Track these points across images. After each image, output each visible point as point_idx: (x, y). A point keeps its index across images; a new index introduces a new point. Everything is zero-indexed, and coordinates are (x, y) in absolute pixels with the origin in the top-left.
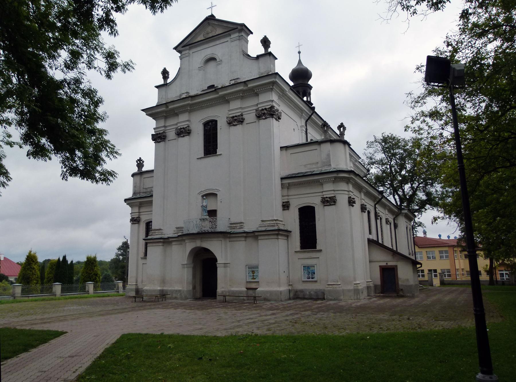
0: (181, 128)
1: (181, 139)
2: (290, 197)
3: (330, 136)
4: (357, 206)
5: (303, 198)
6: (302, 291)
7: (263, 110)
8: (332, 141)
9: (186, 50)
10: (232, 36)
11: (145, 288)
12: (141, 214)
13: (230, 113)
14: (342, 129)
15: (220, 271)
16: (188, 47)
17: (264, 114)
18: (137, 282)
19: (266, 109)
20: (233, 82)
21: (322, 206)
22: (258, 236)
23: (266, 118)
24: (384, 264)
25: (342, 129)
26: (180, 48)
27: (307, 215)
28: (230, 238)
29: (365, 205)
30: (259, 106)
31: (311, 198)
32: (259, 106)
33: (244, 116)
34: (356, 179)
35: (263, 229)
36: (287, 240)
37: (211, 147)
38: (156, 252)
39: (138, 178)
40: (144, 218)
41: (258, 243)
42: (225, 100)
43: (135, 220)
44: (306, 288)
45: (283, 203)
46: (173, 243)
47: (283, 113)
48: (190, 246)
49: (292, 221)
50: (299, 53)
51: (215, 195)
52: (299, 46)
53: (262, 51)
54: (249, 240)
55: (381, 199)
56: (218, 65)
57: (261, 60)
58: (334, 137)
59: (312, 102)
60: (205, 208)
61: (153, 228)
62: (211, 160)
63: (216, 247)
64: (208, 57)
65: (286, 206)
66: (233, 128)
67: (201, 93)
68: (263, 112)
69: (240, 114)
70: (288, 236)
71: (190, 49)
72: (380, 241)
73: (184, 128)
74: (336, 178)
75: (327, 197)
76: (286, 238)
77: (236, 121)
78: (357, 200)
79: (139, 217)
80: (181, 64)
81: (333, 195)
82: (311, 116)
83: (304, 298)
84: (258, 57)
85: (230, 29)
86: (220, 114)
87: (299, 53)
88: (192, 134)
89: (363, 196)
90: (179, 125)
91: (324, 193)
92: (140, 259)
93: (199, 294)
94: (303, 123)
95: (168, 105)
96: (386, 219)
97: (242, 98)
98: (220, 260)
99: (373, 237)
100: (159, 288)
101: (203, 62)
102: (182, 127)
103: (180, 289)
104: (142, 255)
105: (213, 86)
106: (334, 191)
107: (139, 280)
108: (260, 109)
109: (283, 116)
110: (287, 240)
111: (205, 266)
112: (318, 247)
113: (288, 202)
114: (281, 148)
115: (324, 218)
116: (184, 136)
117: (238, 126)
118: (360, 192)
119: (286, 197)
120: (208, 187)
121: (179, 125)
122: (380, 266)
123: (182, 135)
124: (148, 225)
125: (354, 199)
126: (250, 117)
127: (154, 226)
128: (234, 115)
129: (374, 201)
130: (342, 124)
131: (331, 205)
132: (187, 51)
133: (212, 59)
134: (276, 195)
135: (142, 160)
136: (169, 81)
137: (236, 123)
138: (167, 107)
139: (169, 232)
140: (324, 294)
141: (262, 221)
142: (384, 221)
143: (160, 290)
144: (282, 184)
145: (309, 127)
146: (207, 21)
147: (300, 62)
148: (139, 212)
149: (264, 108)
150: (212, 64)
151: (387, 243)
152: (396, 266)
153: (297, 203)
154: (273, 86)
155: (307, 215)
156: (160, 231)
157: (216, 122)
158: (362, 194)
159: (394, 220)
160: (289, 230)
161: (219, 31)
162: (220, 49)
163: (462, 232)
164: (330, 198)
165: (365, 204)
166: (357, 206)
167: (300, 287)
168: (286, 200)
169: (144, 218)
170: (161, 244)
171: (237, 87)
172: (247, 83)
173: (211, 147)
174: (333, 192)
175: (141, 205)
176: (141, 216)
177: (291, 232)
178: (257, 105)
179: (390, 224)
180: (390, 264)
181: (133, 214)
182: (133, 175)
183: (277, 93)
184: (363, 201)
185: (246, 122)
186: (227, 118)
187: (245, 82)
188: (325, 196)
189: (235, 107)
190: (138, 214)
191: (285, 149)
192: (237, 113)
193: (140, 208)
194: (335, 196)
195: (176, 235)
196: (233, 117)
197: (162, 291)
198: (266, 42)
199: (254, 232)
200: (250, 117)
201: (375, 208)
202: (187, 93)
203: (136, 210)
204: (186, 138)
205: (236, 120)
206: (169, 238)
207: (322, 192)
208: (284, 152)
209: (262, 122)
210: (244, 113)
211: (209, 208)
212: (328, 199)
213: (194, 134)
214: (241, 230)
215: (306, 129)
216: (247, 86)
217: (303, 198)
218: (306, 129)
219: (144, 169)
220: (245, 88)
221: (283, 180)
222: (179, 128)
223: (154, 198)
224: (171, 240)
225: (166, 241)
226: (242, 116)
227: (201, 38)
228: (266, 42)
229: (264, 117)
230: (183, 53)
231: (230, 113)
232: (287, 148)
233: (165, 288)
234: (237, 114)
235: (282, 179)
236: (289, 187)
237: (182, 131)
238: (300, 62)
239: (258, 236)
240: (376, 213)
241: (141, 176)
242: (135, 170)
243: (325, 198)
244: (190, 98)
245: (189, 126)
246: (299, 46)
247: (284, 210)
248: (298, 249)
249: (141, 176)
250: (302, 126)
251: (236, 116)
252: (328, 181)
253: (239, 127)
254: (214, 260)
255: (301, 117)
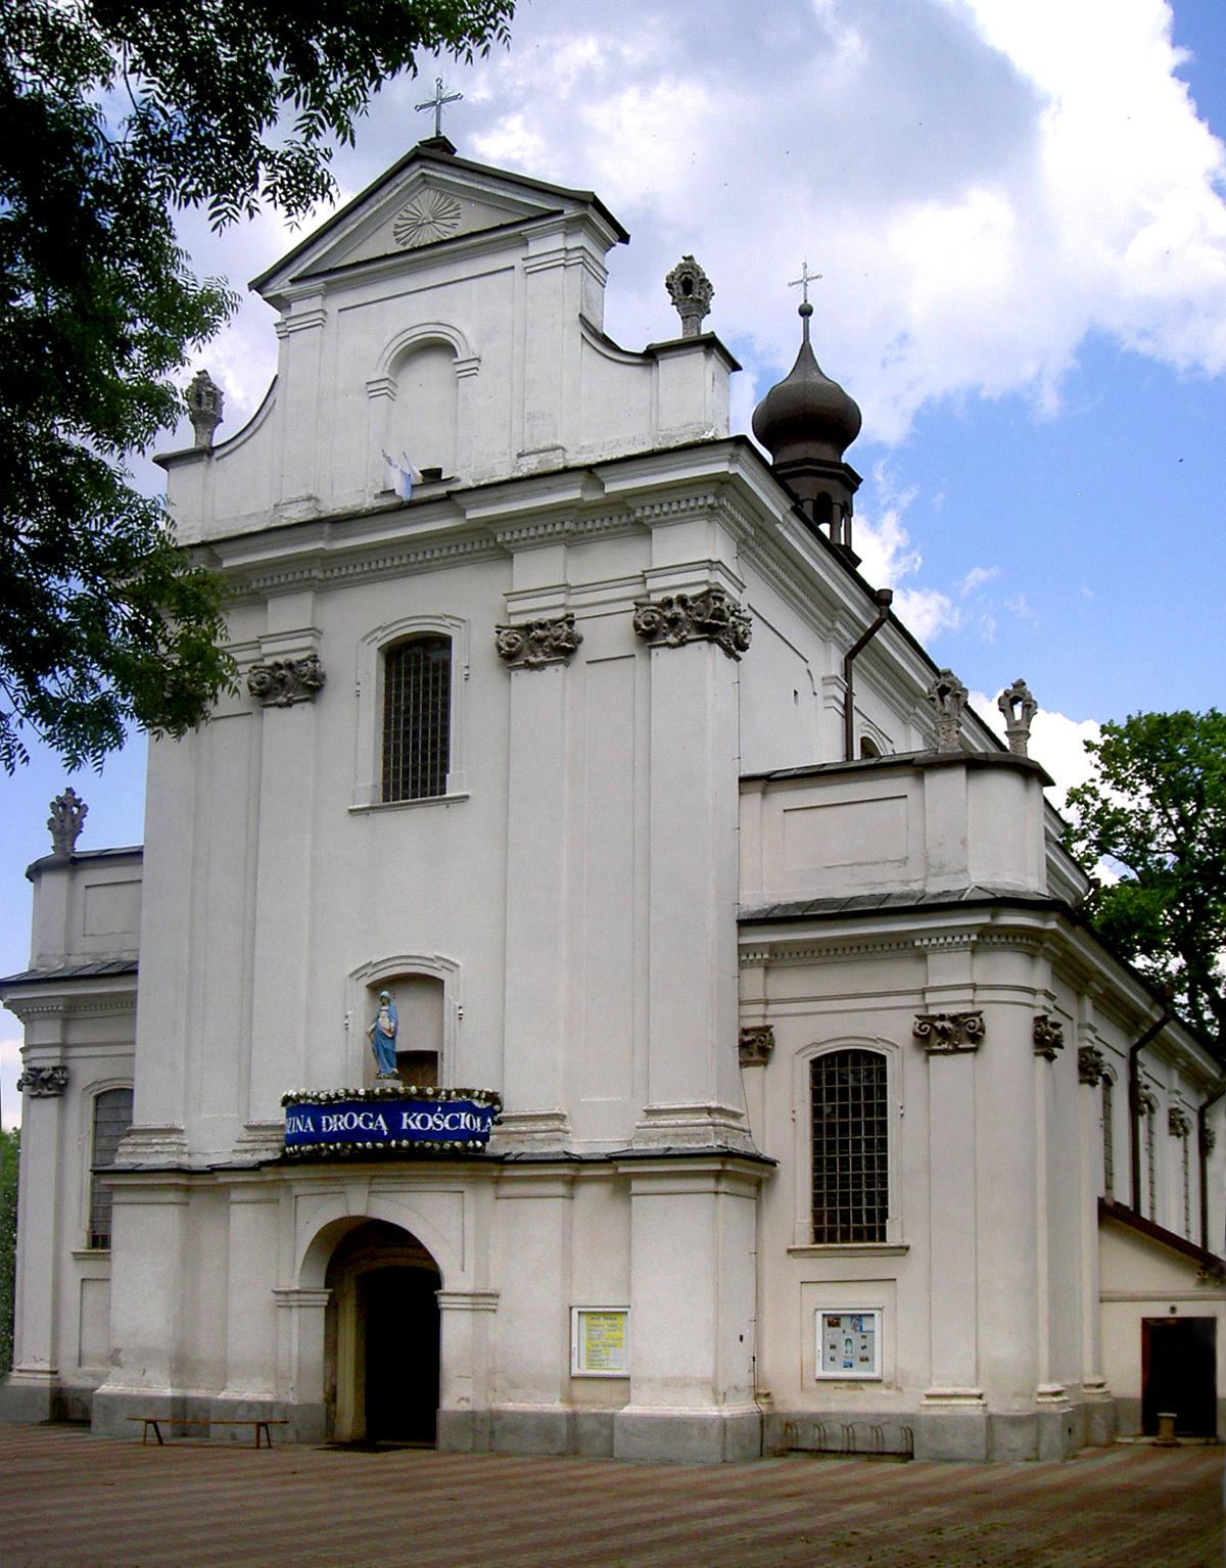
0: (278, 666)
1: (272, 714)
2: (773, 1009)
3: (963, 742)
4: (1067, 1057)
5: (822, 1014)
6: (816, 1421)
7: (668, 603)
8: (975, 765)
9: (309, 296)
10: (535, 248)
11: (105, 1389)
12: (74, 1052)
13: (513, 607)
14: (1018, 709)
15: (455, 1331)
16: (319, 283)
17: (674, 622)
18: (54, 1360)
19: (682, 601)
20: (530, 465)
21: (919, 1058)
22: (628, 1178)
23: (682, 643)
24: (1160, 1311)
25: (1018, 709)
26: (281, 286)
27: (849, 1093)
28: (498, 1181)
29: (1099, 1054)
30: (652, 584)
31: (870, 1010)
32: (652, 584)
33: (580, 628)
34: (1071, 939)
35: (655, 1147)
36: (757, 1198)
37: (416, 761)
38: (147, 1230)
39: (55, 883)
40: (89, 1072)
41: (630, 1201)
42: (491, 545)
43: (45, 1081)
44: (833, 1407)
45: (745, 1032)
46: (235, 1195)
47: (755, 621)
48: (322, 1207)
49: (780, 1119)
50: (806, 312)
51: (433, 984)
52: (805, 282)
53: (670, 326)
54: (591, 1195)
55: (1158, 1026)
56: (459, 376)
57: (668, 366)
58: (979, 746)
59: (856, 549)
60: (388, 1045)
61: (140, 1119)
62: (414, 822)
63: (437, 1218)
64: (417, 334)
65: (756, 1047)
66: (522, 678)
67: (378, 503)
68: (668, 614)
69: (559, 614)
70: (759, 1184)
71: (329, 291)
72: (1145, 1214)
73: (290, 666)
74: (984, 931)
75: (942, 1017)
76: (752, 1190)
77: (541, 645)
78: (1068, 1032)
79: (64, 1068)
80: (283, 362)
81: (968, 1009)
82: (871, 633)
83: (820, 1453)
84: (652, 356)
85: (529, 214)
86: (468, 607)
87: (806, 312)
88: (328, 696)
89: (1090, 1015)
90: (266, 649)
91: (930, 998)
92: (67, 1259)
93: (349, 1420)
94: (836, 670)
95: (217, 550)
96: (1172, 1112)
97: (574, 540)
98: (455, 1279)
99: (1123, 1196)
100: (168, 1392)
101: (390, 354)
102: (281, 660)
103: (268, 1398)
104: (78, 1239)
105: (433, 476)
106: (974, 987)
107: (69, 1350)
108: (657, 598)
109: (758, 636)
110: (757, 1198)
111: (386, 1300)
112: (892, 1239)
113: (767, 1028)
114: (743, 780)
115: (923, 1104)
116: (289, 704)
117: (550, 670)
118: (1079, 994)
119: (759, 1009)
120: (405, 943)
121: (266, 649)
122: (1145, 1322)
123: (281, 699)
124: (114, 1101)
125: (1056, 1025)
126: (606, 632)
127: (144, 1114)
128: (533, 618)
129: (1130, 1033)
130: (1020, 684)
131: (957, 1050)
132: (315, 303)
133: (437, 346)
134: (701, 990)
135: (77, 803)
136: (220, 435)
137: (542, 658)
138: (216, 560)
139: (216, 1142)
140: (910, 1434)
141: (650, 1113)
142: (1161, 1119)
143: (174, 1399)
144: (742, 948)
145: (858, 686)
146: (415, 171)
147: (806, 355)
148: (65, 1046)
149: (673, 595)
150: (432, 369)
151: (1172, 1217)
152: (1208, 1325)
153: (803, 1035)
154: (717, 496)
155: (849, 1093)
156: (174, 1138)
157: (444, 642)
158: (1088, 1003)
159: (1202, 1114)
160: (768, 1154)
161: (473, 218)
162: (471, 303)
163: (1213, 957)
164: (954, 1019)
165: (1099, 1046)
166: (1067, 1057)
167: (797, 1402)
168: (759, 1023)
169: (89, 1072)
170: (172, 1197)
171: (550, 490)
172: (600, 473)
173: (416, 761)
174: (968, 994)
175: (71, 1012)
176: (71, 1064)
177: (773, 1163)
178: (643, 578)
179: (1108, 1082)
180: (1186, 1310)
181: (34, 1053)
182: (35, 872)
183: (733, 527)
184: (1090, 1035)
185: (584, 652)
186: (499, 629)
187: (589, 469)
188: (933, 1011)
189: (540, 579)
190: (57, 1052)
191: (760, 785)
192: (545, 608)
193: (67, 1022)
194: (978, 1014)
195: (250, 1159)
196: (528, 628)
197: (180, 1405)
198: (689, 288)
199: (611, 1159)
200: (606, 632)
201: (1133, 1064)
202: (309, 499)
203: (50, 1032)
204: (301, 714)
205: (540, 641)
206: (213, 1170)
207: (923, 992)
208: (754, 799)
209: (662, 657)
210: (578, 614)
211: (402, 1046)
212: (947, 1024)
213: (336, 696)
214: (554, 1149)
215: (849, 695)
216: (602, 486)
217: (822, 1014)
218: (849, 695)
219: (86, 843)
220: (593, 496)
221: (746, 930)
222: (269, 662)
223: (144, 983)
224: (223, 1179)
225: (197, 1184)
226: (571, 624)
227: (383, 242)
228: (689, 288)
229: (671, 639)
230: (297, 308)
231: (513, 607)
232: (768, 782)
233: (193, 1393)
234: (546, 616)
235: (745, 924)
236: (775, 959)
237: (282, 681)
238: (806, 355)
239: (628, 1178)
240: (1134, 1085)
241: (73, 878)
242: (44, 846)
243: (934, 1018)
244: (327, 528)
245: (315, 659)
246: (805, 282)
247: (744, 1064)
248: (805, 1239)
249: (73, 878)
250: (827, 681)
251: (542, 626)
252: (948, 942)
253: (553, 675)
254: (429, 1277)
255: (826, 635)
